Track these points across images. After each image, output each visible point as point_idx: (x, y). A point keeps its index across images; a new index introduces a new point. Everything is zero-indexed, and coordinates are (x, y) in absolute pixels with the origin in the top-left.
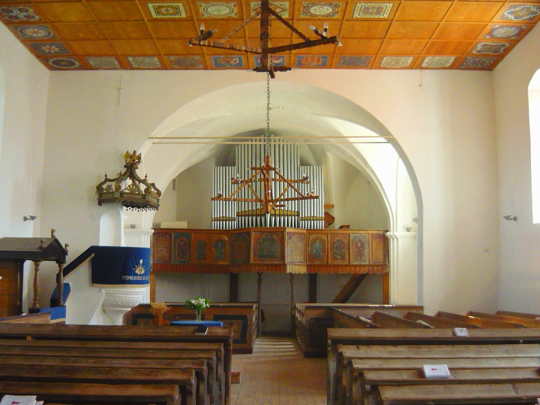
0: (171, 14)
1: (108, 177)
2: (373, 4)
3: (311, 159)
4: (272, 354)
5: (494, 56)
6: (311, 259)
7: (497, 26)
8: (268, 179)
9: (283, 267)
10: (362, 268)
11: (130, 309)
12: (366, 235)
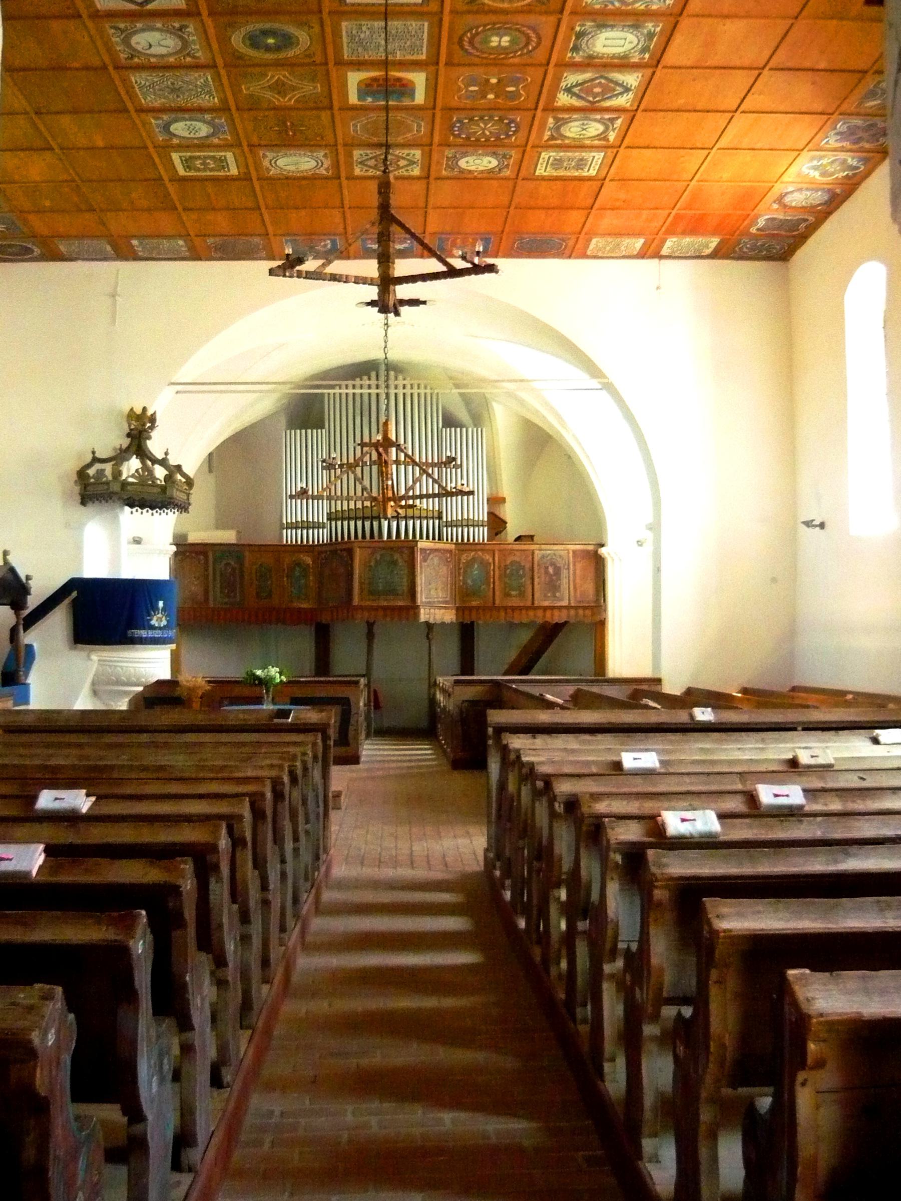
0: (212, 170)
1: (97, 455)
2: (569, 154)
3: (462, 414)
4: (394, 765)
5: (788, 237)
6: (463, 596)
7: (790, 189)
8: (386, 462)
10: (556, 612)
11: (141, 689)
12: (563, 553)
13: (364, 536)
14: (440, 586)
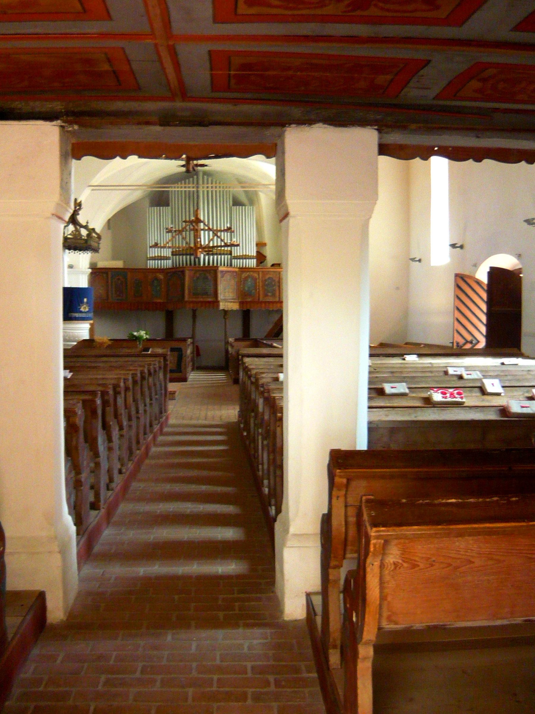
3: (243, 198)
8: (197, 230)
9: (215, 304)
11: (75, 343)
13: (191, 264)
14: (231, 291)
